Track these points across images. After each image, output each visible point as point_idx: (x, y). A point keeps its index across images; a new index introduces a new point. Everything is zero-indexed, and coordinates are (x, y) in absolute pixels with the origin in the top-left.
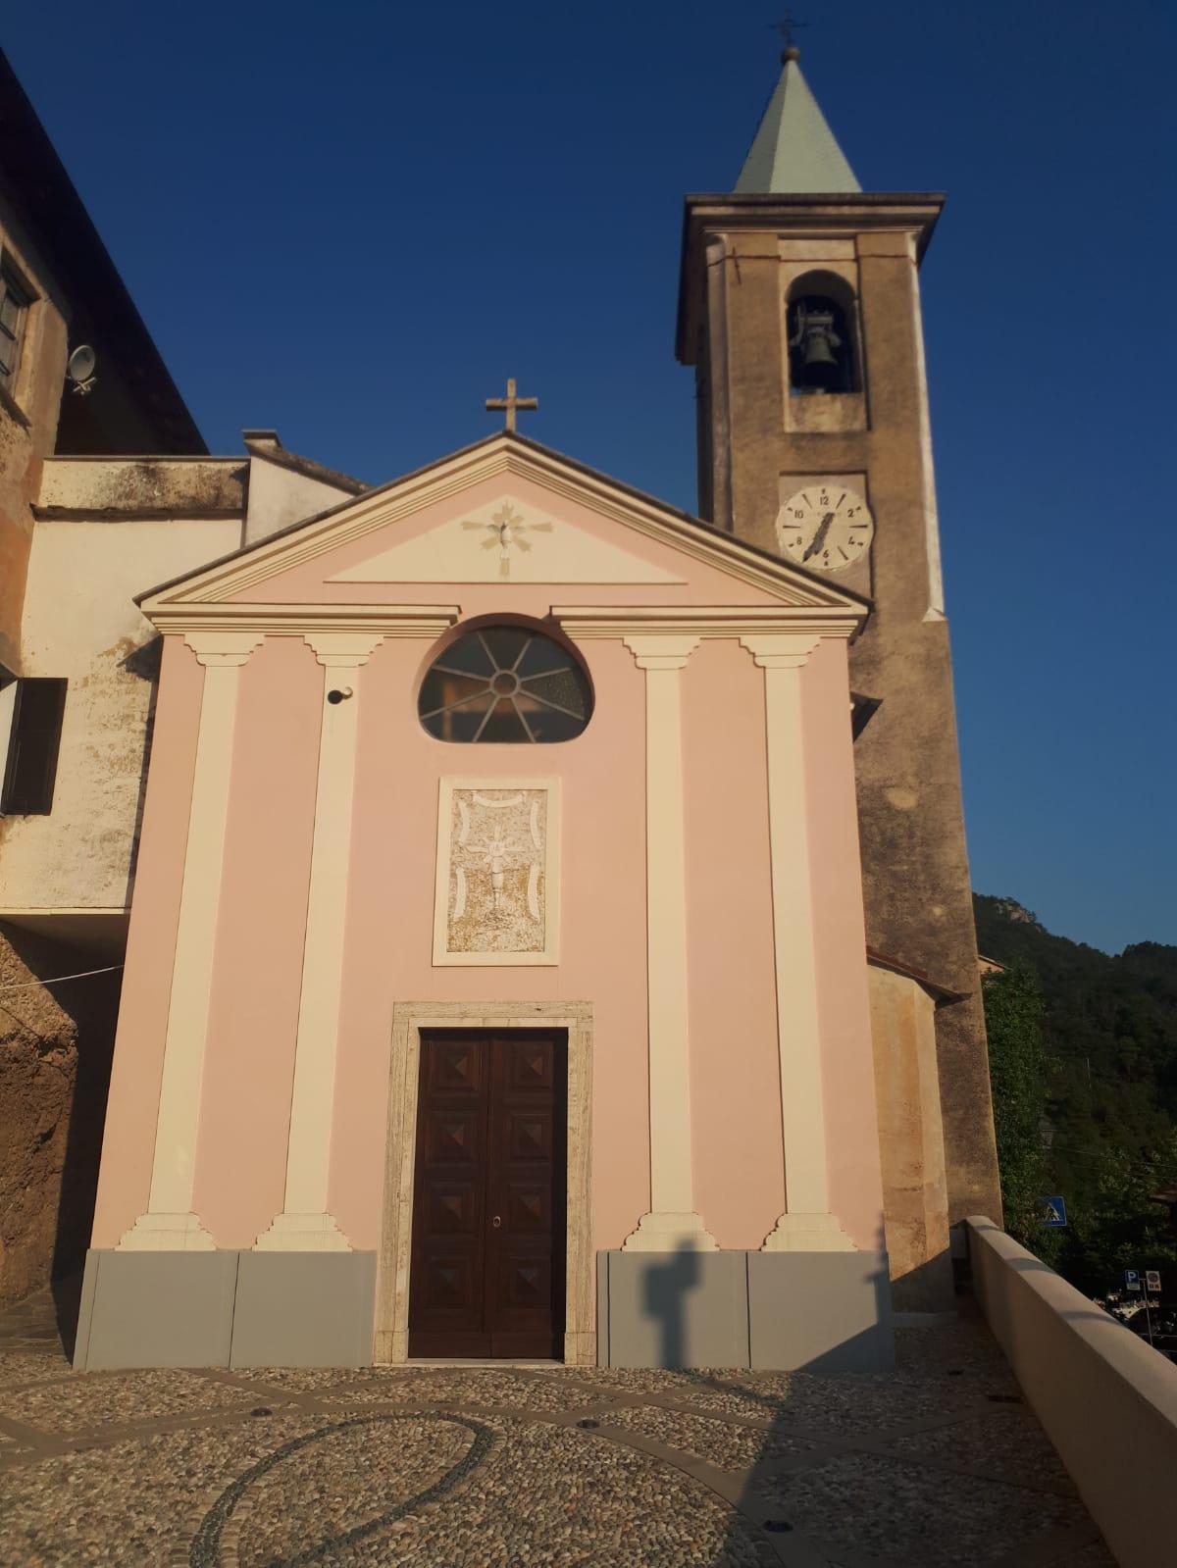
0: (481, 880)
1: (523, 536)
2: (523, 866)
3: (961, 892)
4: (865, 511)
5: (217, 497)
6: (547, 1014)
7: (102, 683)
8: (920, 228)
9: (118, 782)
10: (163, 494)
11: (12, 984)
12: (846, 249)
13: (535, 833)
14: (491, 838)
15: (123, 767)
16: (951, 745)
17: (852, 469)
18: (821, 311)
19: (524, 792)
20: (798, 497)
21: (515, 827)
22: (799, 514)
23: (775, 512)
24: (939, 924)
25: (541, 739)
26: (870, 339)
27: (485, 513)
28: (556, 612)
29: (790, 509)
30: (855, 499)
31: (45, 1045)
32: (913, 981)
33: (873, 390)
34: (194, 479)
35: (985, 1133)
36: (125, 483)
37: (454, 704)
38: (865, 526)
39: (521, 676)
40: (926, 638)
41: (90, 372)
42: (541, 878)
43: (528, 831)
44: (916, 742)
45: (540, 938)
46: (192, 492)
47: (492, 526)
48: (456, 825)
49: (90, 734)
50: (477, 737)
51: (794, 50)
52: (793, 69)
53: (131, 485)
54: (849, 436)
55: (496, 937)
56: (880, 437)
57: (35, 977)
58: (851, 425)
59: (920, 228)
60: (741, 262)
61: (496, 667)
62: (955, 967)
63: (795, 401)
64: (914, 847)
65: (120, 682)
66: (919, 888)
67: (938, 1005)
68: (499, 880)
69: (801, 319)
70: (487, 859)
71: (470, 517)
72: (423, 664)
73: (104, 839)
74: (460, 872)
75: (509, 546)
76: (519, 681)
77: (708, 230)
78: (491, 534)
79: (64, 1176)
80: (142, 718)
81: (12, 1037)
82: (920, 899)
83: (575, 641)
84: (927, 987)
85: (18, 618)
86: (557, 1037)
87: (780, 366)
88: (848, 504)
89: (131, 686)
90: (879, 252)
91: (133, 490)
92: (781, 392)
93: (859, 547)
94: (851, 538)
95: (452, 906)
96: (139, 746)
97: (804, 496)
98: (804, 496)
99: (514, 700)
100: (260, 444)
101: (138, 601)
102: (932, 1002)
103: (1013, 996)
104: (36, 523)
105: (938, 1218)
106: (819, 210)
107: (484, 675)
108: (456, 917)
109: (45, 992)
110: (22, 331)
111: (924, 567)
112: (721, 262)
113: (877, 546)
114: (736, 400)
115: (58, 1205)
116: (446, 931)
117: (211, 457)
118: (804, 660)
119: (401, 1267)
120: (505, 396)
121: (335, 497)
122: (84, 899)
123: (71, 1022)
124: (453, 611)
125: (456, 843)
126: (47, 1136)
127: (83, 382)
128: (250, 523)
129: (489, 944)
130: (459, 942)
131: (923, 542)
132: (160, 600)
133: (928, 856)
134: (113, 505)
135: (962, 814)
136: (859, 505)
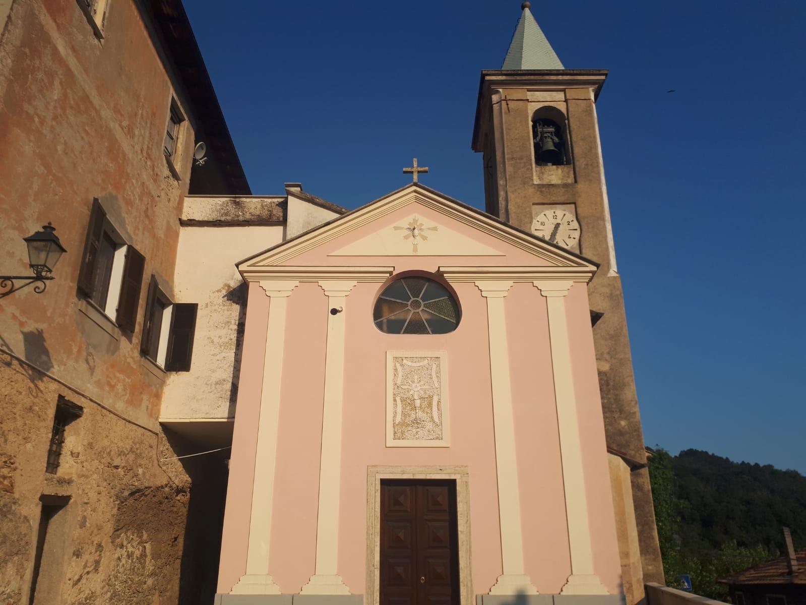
0: (409, 403)
1: (424, 233)
2: (429, 396)
3: (634, 413)
4: (575, 222)
5: (270, 216)
7: (215, 305)
8: (596, 86)
9: (224, 354)
10: (243, 214)
11: (166, 458)
12: (560, 96)
13: (435, 379)
14: (413, 382)
16: (625, 339)
18: (549, 126)
19: (428, 358)
20: (542, 215)
21: (425, 376)
22: (543, 224)
23: (531, 222)
26: (574, 139)
27: (405, 222)
28: (442, 269)
29: (538, 221)
30: (570, 216)
31: (179, 491)
32: (619, 458)
33: (577, 163)
34: (259, 206)
35: (653, 538)
36: (225, 208)
37: (387, 316)
38: (576, 230)
40: (609, 285)
41: (202, 155)
42: (439, 402)
44: (607, 337)
45: (440, 433)
46: (258, 213)
47: (409, 228)
48: (395, 375)
49: (209, 331)
50: (403, 331)
51: (528, 3)
52: (527, 11)
53: (228, 209)
54: (565, 186)
55: (417, 432)
56: (581, 186)
57: (175, 455)
58: (567, 180)
59: (596, 86)
60: (509, 102)
61: (411, 297)
62: (633, 452)
63: (539, 168)
64: (610, 390)
66: (613, 411)
67: (632, 470)
68: (418, 403)
69: (540, 130)
70: (411, 393)
71: (397, 224)
72: (375, 298)
73: (217, 383)
74: (398, 399)
75: (417, 238)
76: (422, 304)
77: (493, 87)
79: (182, 560)
80: (235, 324)
81: (166, 485)
82: (614, 417)
83: (451, 284)
84: (627, 461)
85: (173, 274)
86: (451, 485)
87: (530, 153)
88: (566, 219)
89: (229, 307)
90: (576, 97)
91: (228, 212)
92: (531, 165)
93: (573, 240)
94: (569, 235)
95: (395, 416)
96: (234, 336)
97: (545, 215)
98: (545, 215)
99: (420, 313)
100: (293, 189)
101: (237, 265)
102: (629, 469)
103: (658, 468)
104: (181, 228)
105: (638, 581)
106: (547, 77)
107: (405, 301)
108: (397, 422)
109: (179, 463)
110: (176, 136)
111: (607, 249)
112: (499, 102)
113: (583, 240)
114: (509, 169)
115: (179, 576)
116: (392, 429)
117: (252, 196)
118: (566, 293)
119: (376, 603)
120: (413, 167)
121: (331, 216)
122: (207, 414)
123: (189, 479)
124: (392, 269)
126: (176, 539)
127: (201, 159)
128: (288, 228)
129: (414, 436)
130: (399, 434)
131: (606, 237)
132: (248, 265)
133: (617, 395)
134: (219, 219)
135: (633, 373)
136: (573, 219)
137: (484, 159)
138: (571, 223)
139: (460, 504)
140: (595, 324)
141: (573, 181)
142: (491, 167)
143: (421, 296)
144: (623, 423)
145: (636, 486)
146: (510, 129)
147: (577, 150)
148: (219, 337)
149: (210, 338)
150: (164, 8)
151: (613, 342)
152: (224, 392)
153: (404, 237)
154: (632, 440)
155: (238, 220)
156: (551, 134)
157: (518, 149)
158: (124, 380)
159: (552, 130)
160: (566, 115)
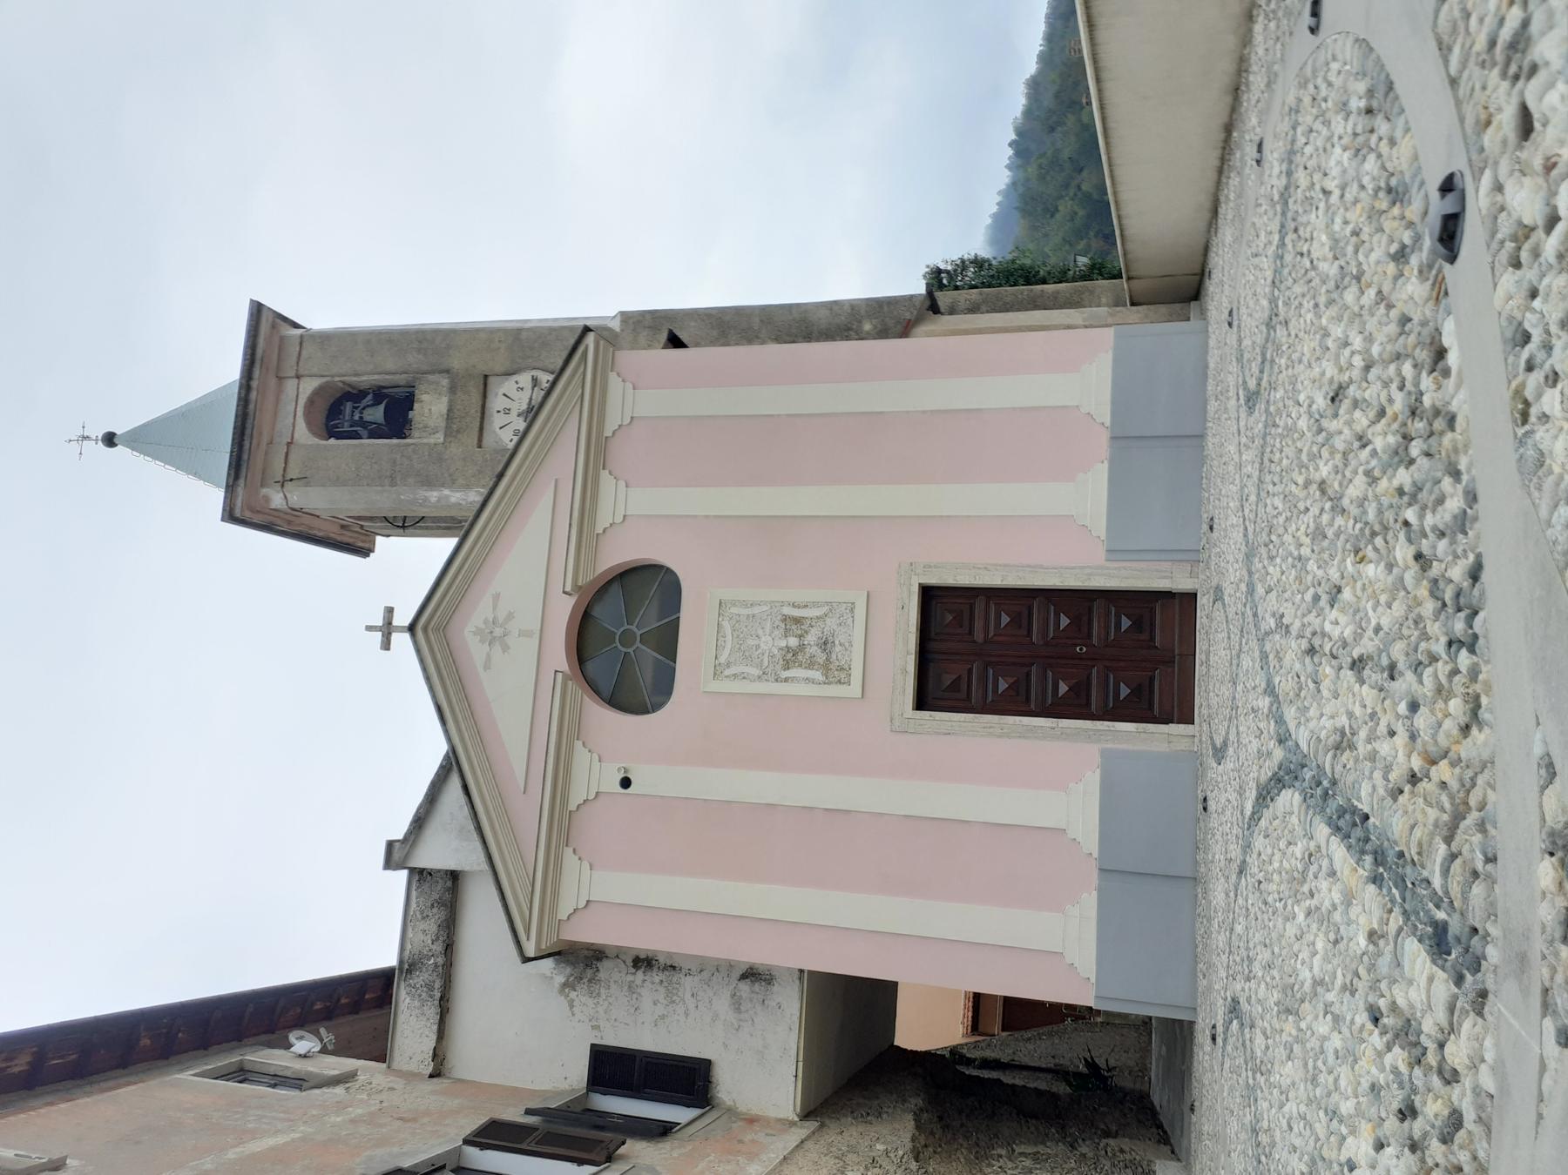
0: (792, 657)
6: (907, 601)
9: (688, 996)
12: (291, 385)
13: (756, 610)
14: (758, 647)
17: (482, 387)
18: (341, 412)
24: (879, 326)
25: (678, 610)
28: (568, 589)
30: (509, 386)
49: (643, 1023)
54: (453, 389)
56: (456, 362)
63: (415, 433)
65: (599, 995)
68: (793, 642)
73: (738, 1010)
76: (626, 627)
78: (497, 648)
83: (596, 574)
92: (409, 445)
108: (822, 678)
124: (560, 676)
125: (759, 677)
134: (437, 1002)
138: (520, 385)
139: (958, 578)
141: (445, 375)
142: (404, 522)
145: (974, 309)
146: (338, 478)
148: (655, 1004)
150: (16, 1070)
151: (732, 331)
153: (504, 652)
154: (895, 313)
155: (443, 966)
158: (710, 1162)
159: (349, 405)
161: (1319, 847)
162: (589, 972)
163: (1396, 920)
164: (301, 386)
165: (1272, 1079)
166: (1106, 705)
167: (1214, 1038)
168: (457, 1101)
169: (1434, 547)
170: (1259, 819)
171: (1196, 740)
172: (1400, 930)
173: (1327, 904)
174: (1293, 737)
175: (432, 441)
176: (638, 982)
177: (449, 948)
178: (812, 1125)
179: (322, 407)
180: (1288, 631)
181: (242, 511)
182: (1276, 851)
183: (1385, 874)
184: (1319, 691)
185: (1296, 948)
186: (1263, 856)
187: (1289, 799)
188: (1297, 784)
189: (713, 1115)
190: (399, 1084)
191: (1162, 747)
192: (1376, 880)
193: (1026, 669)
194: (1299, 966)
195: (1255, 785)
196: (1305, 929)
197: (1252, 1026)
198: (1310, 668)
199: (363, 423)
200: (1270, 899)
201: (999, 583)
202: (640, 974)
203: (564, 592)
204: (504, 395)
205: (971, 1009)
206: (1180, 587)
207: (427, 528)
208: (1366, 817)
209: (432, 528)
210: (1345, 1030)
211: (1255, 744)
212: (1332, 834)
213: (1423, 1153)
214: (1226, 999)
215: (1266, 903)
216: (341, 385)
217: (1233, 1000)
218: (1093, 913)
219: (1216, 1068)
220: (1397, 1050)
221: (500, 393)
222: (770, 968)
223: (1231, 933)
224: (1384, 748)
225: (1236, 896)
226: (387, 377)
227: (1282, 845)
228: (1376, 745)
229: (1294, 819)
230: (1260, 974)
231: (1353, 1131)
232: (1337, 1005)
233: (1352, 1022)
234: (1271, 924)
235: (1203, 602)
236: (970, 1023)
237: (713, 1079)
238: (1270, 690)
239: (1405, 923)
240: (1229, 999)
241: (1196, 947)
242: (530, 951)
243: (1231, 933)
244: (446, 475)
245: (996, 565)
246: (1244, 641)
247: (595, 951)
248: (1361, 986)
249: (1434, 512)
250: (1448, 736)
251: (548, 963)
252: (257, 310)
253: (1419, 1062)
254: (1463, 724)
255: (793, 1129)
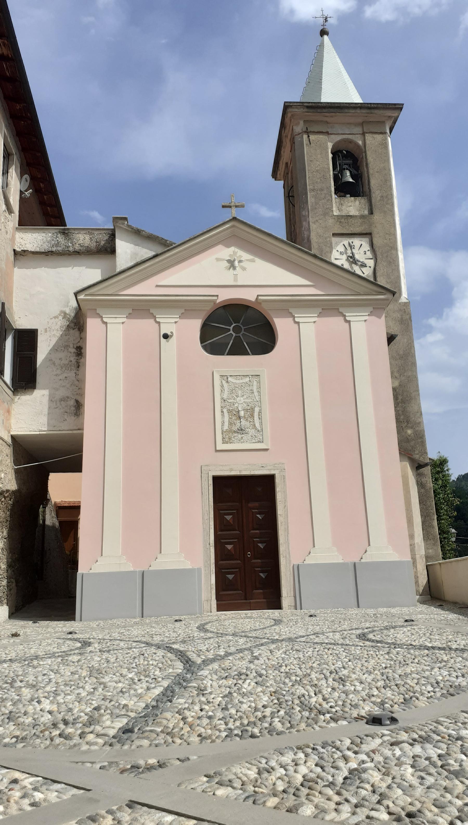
7: (53, 330)
9: (65, 375)
12: (359, 130)
14: (237, 396)
15: (67, 368)
17: (365, 232)
23: (331, 252)
26: (371, 171)
30: (366, 247)
33: (373, 195)
35: (433, 527)
39: (230, 329)
42: (260, 412)
43: (253, 393)
46: (86, 245)
48: (222, 391)
54: (362, 217)
55: (242, 438)
56: (377, 217)
58: (364, 211)
63: (338, 200)
68: (242, 413)
73: (61, 400)
74: (225, 410)
76: (243, 328)
111: (399, 277)
114: (311, 200)
122: (54, 426)
134: (50, 249)
137: (284, 188)
140: (390, 343)
142: (292, 196)
143: (241, 321)
144: (409, 432)
145: (420, 485)
147: (374, 183)
149: (52, 360)
152: (69, 407)
155: (69, 251)
156: (350, 166)
157: (319, 181)
159: (350, 162)
160: (363, 148)
161: (159, 683)
162: (72, 325)
163: (133, 715)
164: (359, 135)
165: (61, 665)
166: (223, 569)
167: (70, 633)
168: (4, 266)
169: (266, 722)
170: (171, 653)
171: (209, 614)
172: (129, 716)
173: (137, 687)
174: (205, 668)
175: (334, 209)
176: (70, 350)
177: (77, 253)
178: (9, 440)
179: (350, 147)
180: (250, 662)
181: (291, 112)
182: (157, 662)
183: (149, 710)
184: (222, 679)
185: (118, 674)
186: (154, 656)
187: (179, 667)
188: (185, 671)
189: (10, 393)
190: (9, 236)
191: (204, 596)
192: (147, 706)
193: (237, 528)
194: (110, 676)
195: (186, 649)
196: (126, 678)
197: (80, 654)
198: (233, 674)
199: (342, 171)
200: (136, 660)
201: (279, 513)
202: (73, 350)
203: (258, 296)
204: (361, 245)
205: (69, 505)
206: (283, 601)
207: (289, 209)
208: (171, 701)
209: (289, 211)
210: (89, 697)
211: (204, 648)
212: (164, 687)
213: (53, 728)
214: (89, 639)
215: (135, 658)
216: (361, 157)
217: (90, 643)
218: (123, 569)
219: (57, 634)
220: (86, 717)
221: (362, 243)
222: (83, 414)
223: (119, 640)
224: (197, 708)
225: (136, 642)
226: (367, 181)
227: (160, 665)
228: (198, 705)
229: (171, 670)
230: (104, 657)
231: (52, 702)
232: (98, 694)
233: (93, 700)
234: (126, 661)
235: (275, 613)
236: (62, 505)
237: (26, 391)
238: (228, 654)
239: (132, 718)
240: (90, 641)
241: (111, 620)
242: (81, 297)
243: (119, 640)
244: (317, 218)
245: (287, 511)
246: (252, 639)
247: (83, 327)
248: (107, 703)
249: (279, 721)
250: (198, 730)
251: (75, 304)
252: (398, 107)
253: (84, 725)
254: (202, 735)
255: (7, 432)
